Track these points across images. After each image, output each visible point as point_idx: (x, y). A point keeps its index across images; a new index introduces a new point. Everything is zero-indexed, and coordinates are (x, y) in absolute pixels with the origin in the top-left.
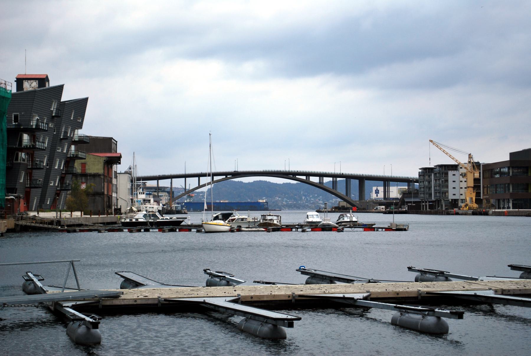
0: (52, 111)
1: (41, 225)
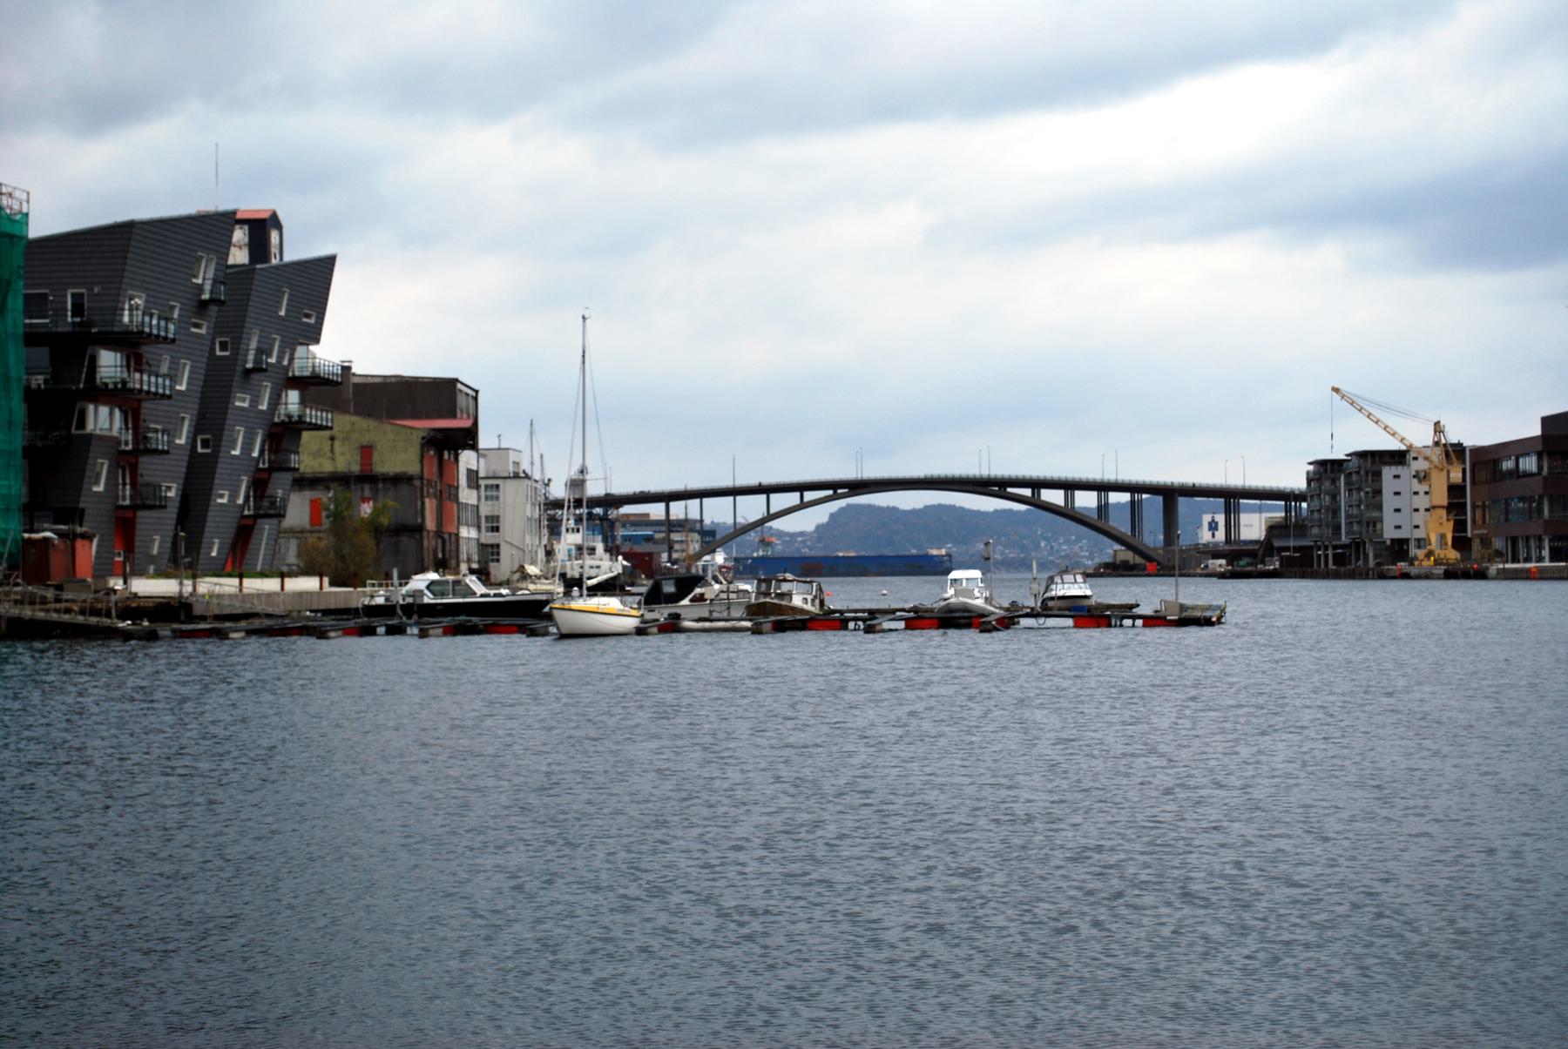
0: (200, 288)
1: (93, 620)
